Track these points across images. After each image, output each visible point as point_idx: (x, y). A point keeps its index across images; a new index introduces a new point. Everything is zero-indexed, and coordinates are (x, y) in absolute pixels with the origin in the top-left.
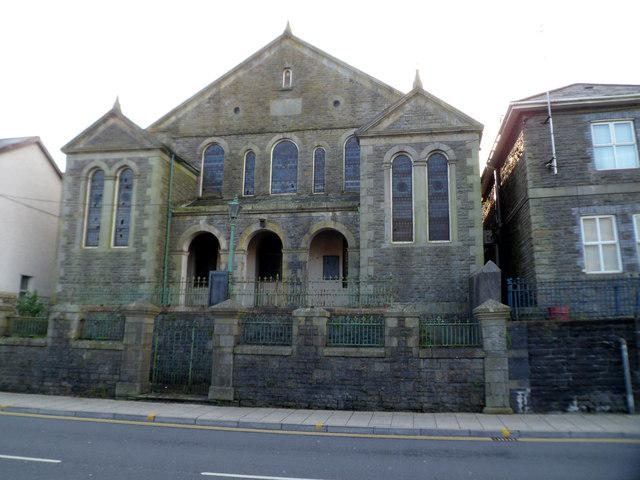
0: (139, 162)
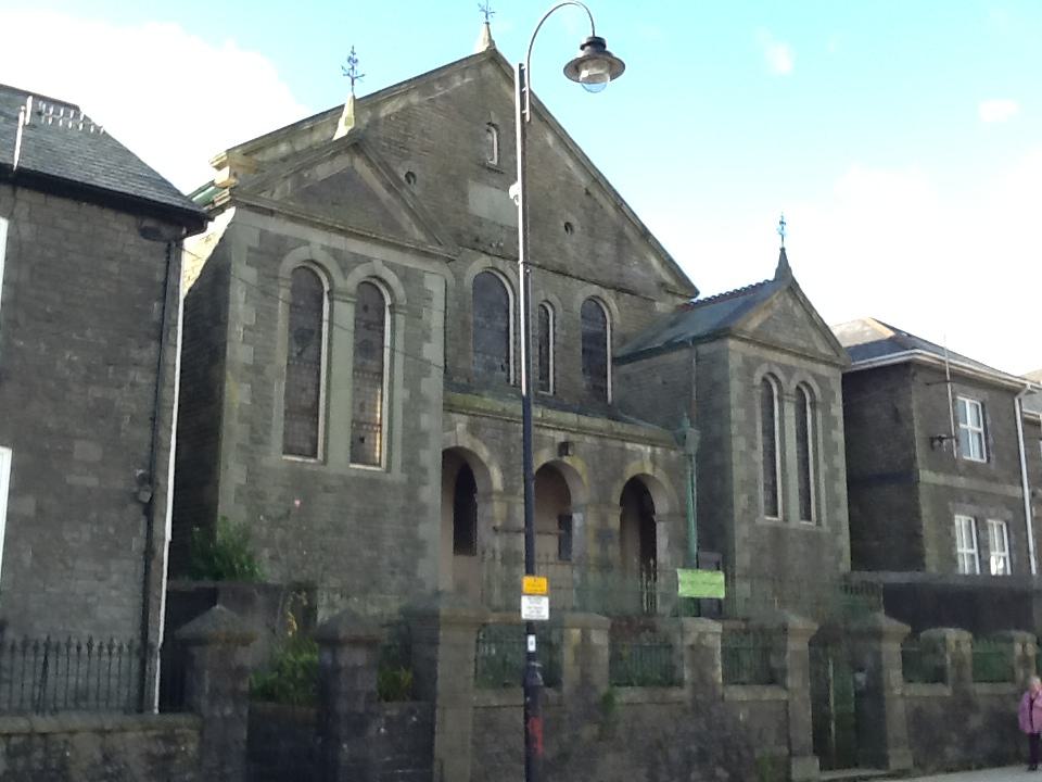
0: (406, 276)
